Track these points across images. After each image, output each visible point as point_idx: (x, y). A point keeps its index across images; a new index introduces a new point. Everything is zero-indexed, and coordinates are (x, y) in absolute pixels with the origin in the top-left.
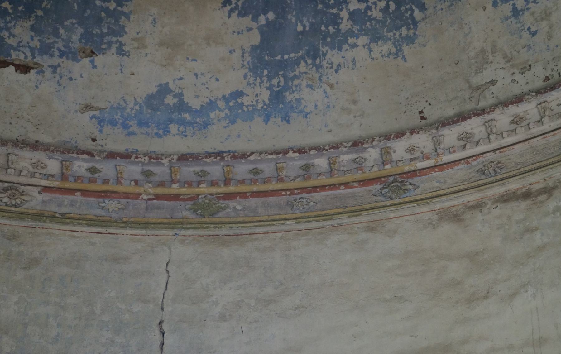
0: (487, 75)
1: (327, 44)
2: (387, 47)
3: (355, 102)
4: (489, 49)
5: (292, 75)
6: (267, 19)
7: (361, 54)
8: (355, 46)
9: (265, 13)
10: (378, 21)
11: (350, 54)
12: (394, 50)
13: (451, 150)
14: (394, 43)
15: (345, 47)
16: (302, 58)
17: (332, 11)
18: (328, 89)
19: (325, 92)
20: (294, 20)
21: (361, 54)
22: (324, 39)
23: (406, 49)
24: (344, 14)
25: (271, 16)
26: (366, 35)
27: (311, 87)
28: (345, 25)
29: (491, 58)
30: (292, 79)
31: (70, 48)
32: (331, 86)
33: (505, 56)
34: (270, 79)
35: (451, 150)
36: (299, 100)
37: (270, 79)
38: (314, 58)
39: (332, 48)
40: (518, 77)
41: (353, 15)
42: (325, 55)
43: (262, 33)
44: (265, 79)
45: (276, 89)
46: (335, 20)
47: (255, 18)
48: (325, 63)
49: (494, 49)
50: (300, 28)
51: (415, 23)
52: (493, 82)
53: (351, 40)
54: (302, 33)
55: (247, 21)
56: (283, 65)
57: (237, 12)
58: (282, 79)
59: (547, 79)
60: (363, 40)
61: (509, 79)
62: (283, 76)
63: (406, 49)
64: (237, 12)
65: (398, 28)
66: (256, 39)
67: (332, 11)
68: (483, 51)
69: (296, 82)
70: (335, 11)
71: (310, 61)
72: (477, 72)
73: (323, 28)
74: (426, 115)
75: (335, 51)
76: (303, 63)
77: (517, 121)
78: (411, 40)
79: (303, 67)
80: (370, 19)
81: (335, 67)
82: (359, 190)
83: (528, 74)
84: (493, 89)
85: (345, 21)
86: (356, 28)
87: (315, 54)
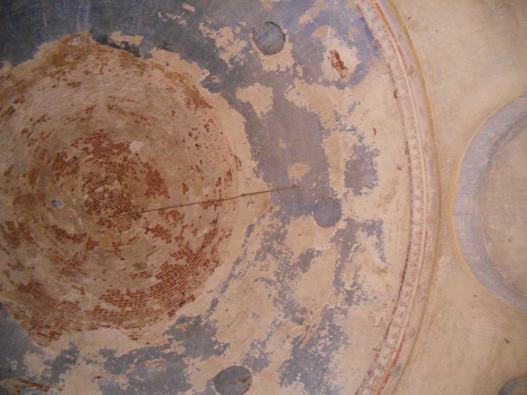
0: (378, 319)
1: (325, 364)
2: (342, 347)
3: (352, 369)
4: (370, 314)
5: (325, 383)
6: (299, 377)
7: (337, 356)
8: (333, 357)
9: (297, 376)
10: (332, 344)
11: (335, 360)
12: (345, 345)
13: (396, 342)
14: (343, 344)
15: (331, 360)
16: (322, 375)
17: (315, 356)
18: (341, 375)
19: (341, 376)
20: (307, 369)
21: (337, 356)
22: (322, 364)
23: (348, 341)
24: (320, 353)
25: (299, 375)
26: (333, 350)
27: (335, 379)
28: (324, 355)
29: (373, 315)
30: (327, 383)
31: (284, 297)
32: (340, 373)
33: (376, 310)
34: (320, 391)
35: (396, 342)
36: (336, 386)
37: (320, 391)
38: (326, 372)
39: (328, 363)
40: (386, 309)
41: (322, 350)
42: (327, 368)
43: (302, 381)
44: (318, 392)
45: (325, 391)
46: (320, 356)
47: (295, 380)
48: (331, 370)
49: (371, 313)
50: (312, 369)
51: (342, 333)
52: (382, 318)
53: (330, 356)
54: (314, 369)
55: (294, 383)
56: (319, 383)
57: (288, 384)
58: (323, 387)
59: (394, 301)
60: (334, 353)
61: (385, 313)
62: (323, 385)
63: (348, 341)
64: (288, 384)
65: (340, 339)
66: (302, 385)
67: (315, 356)
68: (369, 317)
69: (329, 383)
70: (317, 355)
71: (325, 374)
72: (374, 322)
73: (319, 362)
74: (375, 348)
75: (329, 364)
76: (324, 377)
77: (413, 274)
78: (347, 338)
79: (326, 378)
80: (329, 346)
81: (334, 367)
82: (387, 385)
83: (388, 306)
84: (384, 319)
85: (322, 354)
86: (328, 352)
87: (325, 371)
